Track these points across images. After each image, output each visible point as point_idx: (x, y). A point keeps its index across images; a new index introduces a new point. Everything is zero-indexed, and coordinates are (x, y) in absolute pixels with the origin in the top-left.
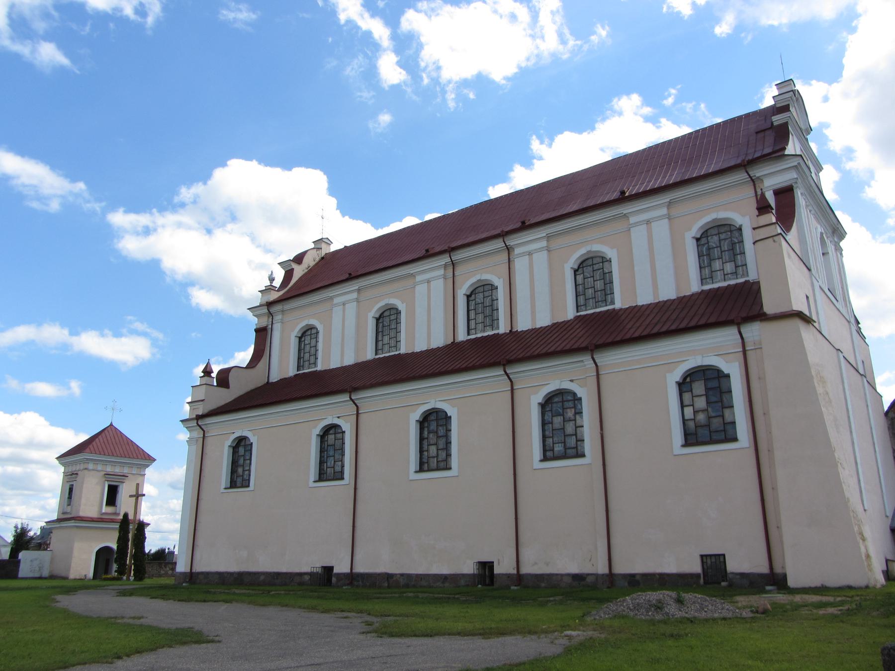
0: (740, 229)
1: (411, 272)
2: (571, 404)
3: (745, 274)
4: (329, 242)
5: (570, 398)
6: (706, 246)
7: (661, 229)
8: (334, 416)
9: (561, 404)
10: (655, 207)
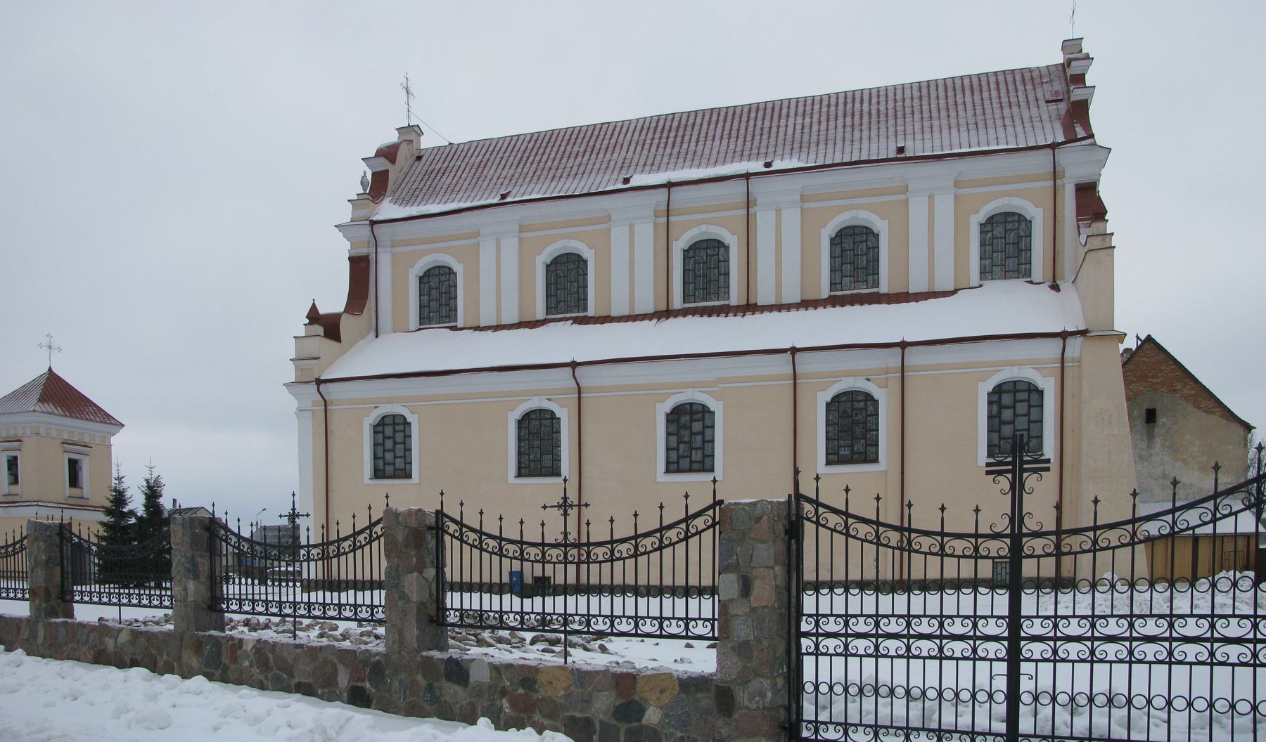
3: (1028, 274)
4: (420, 132)
5: (547, 416)
6: (990, 234)
9: (850, 404)
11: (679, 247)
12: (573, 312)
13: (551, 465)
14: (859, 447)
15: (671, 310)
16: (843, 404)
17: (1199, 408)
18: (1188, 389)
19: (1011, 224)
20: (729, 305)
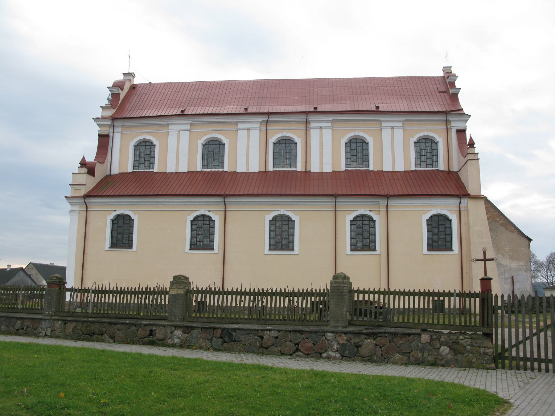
0: (296, 143)
1: (236, 121)
2: (207, 222)
3: (367, 165)
5: (207, 219)
7: (185, 136)
8: (206, 210)
10: (397, 123)
11: (272, 140)
12: (216, 169)
13: (208, 244)
14: (366, 242)
15: (268, 171)
16: (358, 222)
17: (508, 230)
18: (502, 221)
19: (216, 145)
20: (296, 170)
